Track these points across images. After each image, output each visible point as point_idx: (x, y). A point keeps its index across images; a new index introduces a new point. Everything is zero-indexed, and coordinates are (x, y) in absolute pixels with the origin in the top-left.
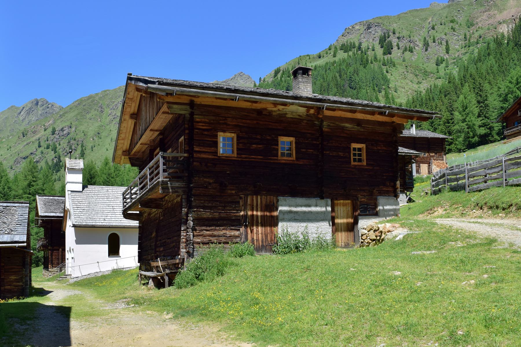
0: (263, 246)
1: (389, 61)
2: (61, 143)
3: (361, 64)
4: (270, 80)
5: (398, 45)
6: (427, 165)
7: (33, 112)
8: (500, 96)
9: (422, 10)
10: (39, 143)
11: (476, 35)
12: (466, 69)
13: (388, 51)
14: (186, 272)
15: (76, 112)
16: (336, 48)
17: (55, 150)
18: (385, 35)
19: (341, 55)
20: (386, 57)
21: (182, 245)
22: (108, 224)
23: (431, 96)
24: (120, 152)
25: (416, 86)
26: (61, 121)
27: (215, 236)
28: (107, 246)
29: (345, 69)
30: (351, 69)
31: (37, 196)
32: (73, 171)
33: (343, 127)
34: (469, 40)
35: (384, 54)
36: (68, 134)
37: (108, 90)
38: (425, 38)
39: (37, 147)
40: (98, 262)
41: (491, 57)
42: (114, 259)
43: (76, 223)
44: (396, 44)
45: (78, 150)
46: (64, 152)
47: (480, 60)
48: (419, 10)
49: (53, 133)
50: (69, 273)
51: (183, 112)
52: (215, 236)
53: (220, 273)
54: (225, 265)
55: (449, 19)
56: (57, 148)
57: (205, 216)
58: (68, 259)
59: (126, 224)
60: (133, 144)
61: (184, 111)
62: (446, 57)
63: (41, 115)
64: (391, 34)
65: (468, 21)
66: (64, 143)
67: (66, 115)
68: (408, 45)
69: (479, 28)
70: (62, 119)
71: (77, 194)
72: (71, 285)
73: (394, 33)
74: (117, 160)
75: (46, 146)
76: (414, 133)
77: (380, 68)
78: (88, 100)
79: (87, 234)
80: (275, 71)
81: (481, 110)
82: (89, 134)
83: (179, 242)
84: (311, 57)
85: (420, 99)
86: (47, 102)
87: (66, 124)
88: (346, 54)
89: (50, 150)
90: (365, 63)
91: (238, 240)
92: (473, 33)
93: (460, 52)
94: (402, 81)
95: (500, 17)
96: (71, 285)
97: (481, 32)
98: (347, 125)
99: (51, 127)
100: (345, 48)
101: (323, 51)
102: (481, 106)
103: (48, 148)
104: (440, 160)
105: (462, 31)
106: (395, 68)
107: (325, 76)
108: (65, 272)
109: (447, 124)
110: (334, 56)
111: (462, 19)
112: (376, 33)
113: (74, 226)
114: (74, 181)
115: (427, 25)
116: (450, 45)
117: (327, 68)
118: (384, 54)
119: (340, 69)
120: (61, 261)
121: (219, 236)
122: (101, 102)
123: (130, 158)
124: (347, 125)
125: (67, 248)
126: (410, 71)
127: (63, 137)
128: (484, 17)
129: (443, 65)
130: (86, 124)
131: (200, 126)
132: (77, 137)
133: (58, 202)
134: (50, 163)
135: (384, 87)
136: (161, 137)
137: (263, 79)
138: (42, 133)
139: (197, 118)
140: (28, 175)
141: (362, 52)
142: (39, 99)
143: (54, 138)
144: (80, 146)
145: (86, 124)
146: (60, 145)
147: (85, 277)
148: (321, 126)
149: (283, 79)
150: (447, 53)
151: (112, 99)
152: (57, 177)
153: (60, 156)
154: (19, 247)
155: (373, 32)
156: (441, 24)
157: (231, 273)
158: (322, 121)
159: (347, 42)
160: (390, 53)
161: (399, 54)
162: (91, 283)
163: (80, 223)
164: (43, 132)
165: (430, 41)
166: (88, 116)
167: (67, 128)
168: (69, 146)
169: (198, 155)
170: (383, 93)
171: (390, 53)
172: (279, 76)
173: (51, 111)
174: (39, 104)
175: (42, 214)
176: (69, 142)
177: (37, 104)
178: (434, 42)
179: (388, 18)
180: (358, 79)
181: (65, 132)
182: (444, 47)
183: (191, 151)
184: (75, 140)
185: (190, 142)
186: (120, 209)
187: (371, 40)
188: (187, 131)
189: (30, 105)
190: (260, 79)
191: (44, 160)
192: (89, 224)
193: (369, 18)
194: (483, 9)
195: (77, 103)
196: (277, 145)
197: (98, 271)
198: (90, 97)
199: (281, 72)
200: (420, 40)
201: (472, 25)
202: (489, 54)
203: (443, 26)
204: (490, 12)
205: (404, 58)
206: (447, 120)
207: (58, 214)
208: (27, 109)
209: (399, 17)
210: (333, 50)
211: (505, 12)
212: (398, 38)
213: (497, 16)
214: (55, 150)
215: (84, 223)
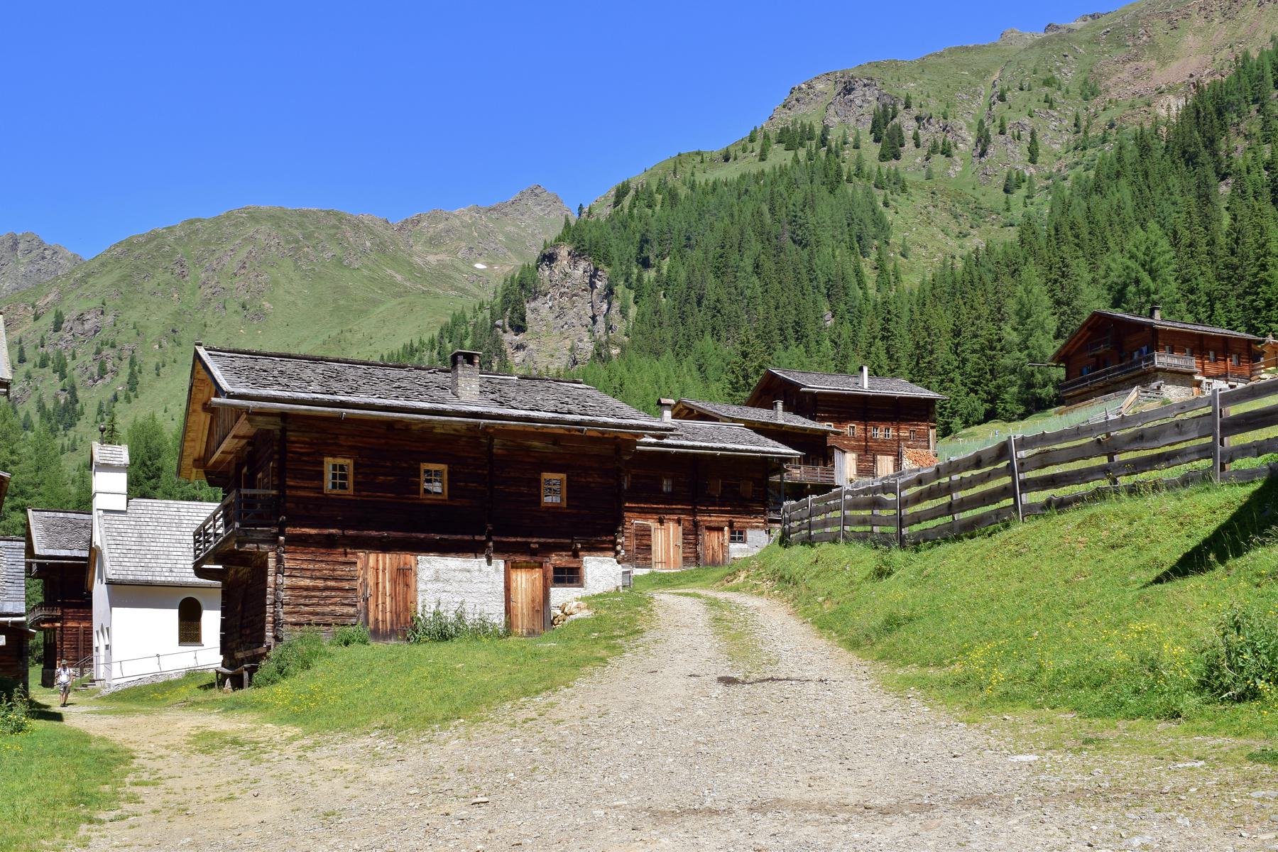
0: (392, 630)
1: (891, 177)
2: (79, 352)
3: (823, 183)
4: (605, 212)
5: (916, 138)
6: (891, 458)
8: (1110, 289)
9: (979, 49)
10: (22, 350)
11: (1103, 119)
12: (1066, 207)
13: (892, 151)
14: (267, 667)
15: (117, 274)
16: (766, 137)
17: (61, 370)
18: (885, 111)
19: (780, 156)
20: (886, 165)
21: (269, 626)
23: (976, 273)
24: (188, 461)
25: (953, 243)
26: (78, 297)
27: (317, 614)
29: (785, 195)
30: (798, 196)
31: (30, 512)
33: (529, 447)
34: (1086, 133)
35: (883, 157)
37: (199, 220)
38: (981, 122)
39: (16, 362)
41: (1123, 182)
42: (190, 649)
44: (911, 133)
45: (121, 374)
46: (85, 378)
47: (1098, 189)
48: (972, 49)
49: (57, 327)
51: (270, 427)
52: (317, 614)
53: (306, 666)
54: (314, 655)
55: (1042, 75)
56: (65, 365)
57: (1134, 393)
60: (209, 452)
61: (274, 426)
62: (1030, 171)
64: (900, 107)
65: (1085, 82)
66: (84, 354)
67: (91, 281)
68: (940, 137)
69: (1110, 102)
70: (80, 291)
72: (103, 698)
73: (908, 106)
74: (184, 473)
75: (38, 360)
76: (866, 386)
77: (868, 194)
78: (147, 242)
80: (618, 190)
81: (1063, 322)
82: (150, 331)
83: (263, 621)
84: (707, 157)
85: (950, 280)
86: (41, 243)
87: (92, 304)
88: (791, 153)
89: (48, 370)
90: (834, 181)
91: (353, 620)
92: (1096, 116)
93: (1064, 162)
94: (921, 229)
95: (1161, 77)
97: (1114, 113)
98: (536, 443)
99: (53, 310)
100: (790, 138)
101: (736, 144)
102: (1063, 314)
104: (921, 447)
105: (1071, 108)
106: (905, 195)
107: (736, 209)
108: (91, 675)
109: (988, 352)
110: (763, 158)
111: (1069, 75)
112: (866, 105)
113: (110, 583)
114: (110, 488)
115: (985, 90)
116: (1040, 143)
117: (741, 189)
118: (883, 157)
119: (772, 193)
120: (82, 652)
121: (324, 614)
122: (180, 250)
123: (207, 473)
124: (536, 443)
126: (940, 204)
128: (1124, 75)
129: (1023, 192)
130: (142, 307)
131: (298, 448)
132: (119, 339)
133: (76, 525)
134: (50, 406)
135: (876, 242)
136: (250, 448)
137: (586, 210)
139: (292, 436)
141: (829, 151)
144: (126, 362)
145: (142, 307)
146: (74, 358)
148: (490, 446)
149: (635, 211)
150: (1033, 160)
151: (209, 243)
152: (66, 442)
153: (73, 388)
154: (13, 623)
155: (858, 102)
156: (1021, 89)
157: (319, 666)
158: (492, 439)
159: (794, 123)
160: (897, 157)
161: (918, 160)
162: (143, 695)
164: (30, 324)
165: (993, 131)
166: (149, 285)
167: (92, 315)
168: (97, 363)
169: (294, 493)
170: (874, 255)
171: (897, 157)
172: (627, 201)
174: (21, 246)
176: (98, 352)
178: (1002, 133)
179: (895, 65)
180: (812, 220)
181: (87, 326)
182: (1025, 145)
183: (281, 487)
184: (113, 346)
185: (281, 472)
186: (190, 561)
187: (852, 122)
188: (276, 457)
190: (581, 208)
191: (34, 398)
192: (141, 578)
193: (849, 65)
194: (1122, 53)
195: (119, 250)
196: (419, 476)
198: (153, 237)
199: (632, 192)
200: (970, 126)
201: (1094, 93)
202: (1118, 175)
203: (1025, 94)
204: (1140, 64)
205: (929, 171)
206: (990, 341)
207: (76, 553)
209: (923, 66)
210: (760, 142)
211: (1174, 65)
212: (918, 119)
213: (1156, 73)
214: (61, 370)
215: (131, 577)
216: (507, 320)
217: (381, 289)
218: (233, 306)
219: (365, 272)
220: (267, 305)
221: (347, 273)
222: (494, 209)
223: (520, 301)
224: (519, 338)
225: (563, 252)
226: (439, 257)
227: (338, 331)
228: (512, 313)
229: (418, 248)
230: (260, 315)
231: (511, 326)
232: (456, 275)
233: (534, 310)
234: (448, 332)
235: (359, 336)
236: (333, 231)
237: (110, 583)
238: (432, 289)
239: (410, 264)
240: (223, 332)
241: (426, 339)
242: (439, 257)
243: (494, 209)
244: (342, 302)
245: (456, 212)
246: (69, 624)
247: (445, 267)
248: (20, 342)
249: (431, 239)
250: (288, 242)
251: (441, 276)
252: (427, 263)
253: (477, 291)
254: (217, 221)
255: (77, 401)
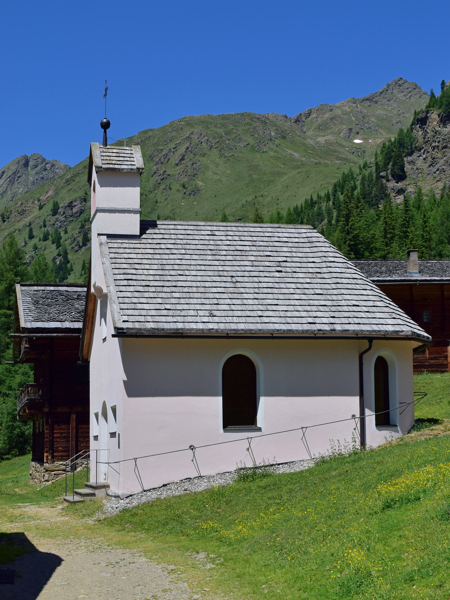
2: (69, 228)
7: (20, 179)
10: (31, 230)
17: (57, 241)
22: (222, 326)
26: (69, 191)
28: (220, 399)
32: (114, 176)
36: (80, 214)
37: (151, 130)
39: (27, 239)
40: (192, 448)
42: (240, 437)
43: (125, 325)
46: (73, 245)
49: (55, 211)
50: (102, 481)
56: (61, 238)
58: (96, 438)
59: (277, 327)
63: (33, 183)
66: (73, 229)
67: (77, 179)
70: (69, 187)
71: (126, 243)
72: (110, 522)
75: (42, 236)
79: (156, 357)
86: (44, 160)
89: (49, 242)
96: (110, 522)
99: (51, 202)
103: (45, 238)
113: (120, 333)
114: (114, 207)
120: (79, 444)
125: (95, 407)
127: (71, 219)
138: (35, 213)
140: (7, 271)
142: (29, 155)
143: (57, 220)
146: (66, 232)
147: (154, 495)
153: (66, 253)
163: (137, 325)
164: (36, 212)
167: (78, 202)
173: (51, 176)
174: (31, 163)
175: (29, 325)
177: (26, 164)
181: (75, 210)
189: (14, 168)
192: (167, 326)
197: (193, 474)
207: (67, 325)
208: (10, 173)
214: (57, 241)
215: (151, 325)
216: (389, 172)
217: (284, 164)
218: (176, 186)
219: (272, 154)
220: (200, 183)
221: (258, 155)
222: (367, 99)
223: (400, 157)
224: (400, 185)
225: (434, 116)
226: (326, 138)
227: (252, 197)
228: (393, 165)
229: (310, 133)
230: (195, 192)
231: (393, 176)
232: (341, 149)
233: (410, 163)
234: (339, 187)
235: (269, 199)
236: (247, 127)
237: (120, 333)
238: (322, 161)
239: (304, 145)
240: (169, 206)
241: (322, 194)
242: (326, 138)
243: (367, 99)
244: (255, 176)
245: (338, 104)
246: (59, 410)
247: (331, 144)
248: (30, 224)
249: (320, 126)
250: (214, 138)
251: (328, 151)
252: (318, 143)
253: (356, 159)
254: (163, 129)
255: (68, 262)
